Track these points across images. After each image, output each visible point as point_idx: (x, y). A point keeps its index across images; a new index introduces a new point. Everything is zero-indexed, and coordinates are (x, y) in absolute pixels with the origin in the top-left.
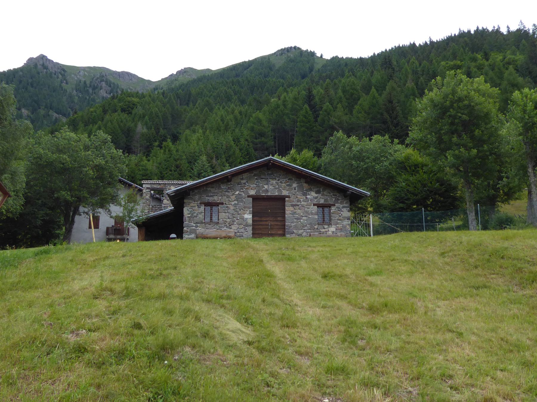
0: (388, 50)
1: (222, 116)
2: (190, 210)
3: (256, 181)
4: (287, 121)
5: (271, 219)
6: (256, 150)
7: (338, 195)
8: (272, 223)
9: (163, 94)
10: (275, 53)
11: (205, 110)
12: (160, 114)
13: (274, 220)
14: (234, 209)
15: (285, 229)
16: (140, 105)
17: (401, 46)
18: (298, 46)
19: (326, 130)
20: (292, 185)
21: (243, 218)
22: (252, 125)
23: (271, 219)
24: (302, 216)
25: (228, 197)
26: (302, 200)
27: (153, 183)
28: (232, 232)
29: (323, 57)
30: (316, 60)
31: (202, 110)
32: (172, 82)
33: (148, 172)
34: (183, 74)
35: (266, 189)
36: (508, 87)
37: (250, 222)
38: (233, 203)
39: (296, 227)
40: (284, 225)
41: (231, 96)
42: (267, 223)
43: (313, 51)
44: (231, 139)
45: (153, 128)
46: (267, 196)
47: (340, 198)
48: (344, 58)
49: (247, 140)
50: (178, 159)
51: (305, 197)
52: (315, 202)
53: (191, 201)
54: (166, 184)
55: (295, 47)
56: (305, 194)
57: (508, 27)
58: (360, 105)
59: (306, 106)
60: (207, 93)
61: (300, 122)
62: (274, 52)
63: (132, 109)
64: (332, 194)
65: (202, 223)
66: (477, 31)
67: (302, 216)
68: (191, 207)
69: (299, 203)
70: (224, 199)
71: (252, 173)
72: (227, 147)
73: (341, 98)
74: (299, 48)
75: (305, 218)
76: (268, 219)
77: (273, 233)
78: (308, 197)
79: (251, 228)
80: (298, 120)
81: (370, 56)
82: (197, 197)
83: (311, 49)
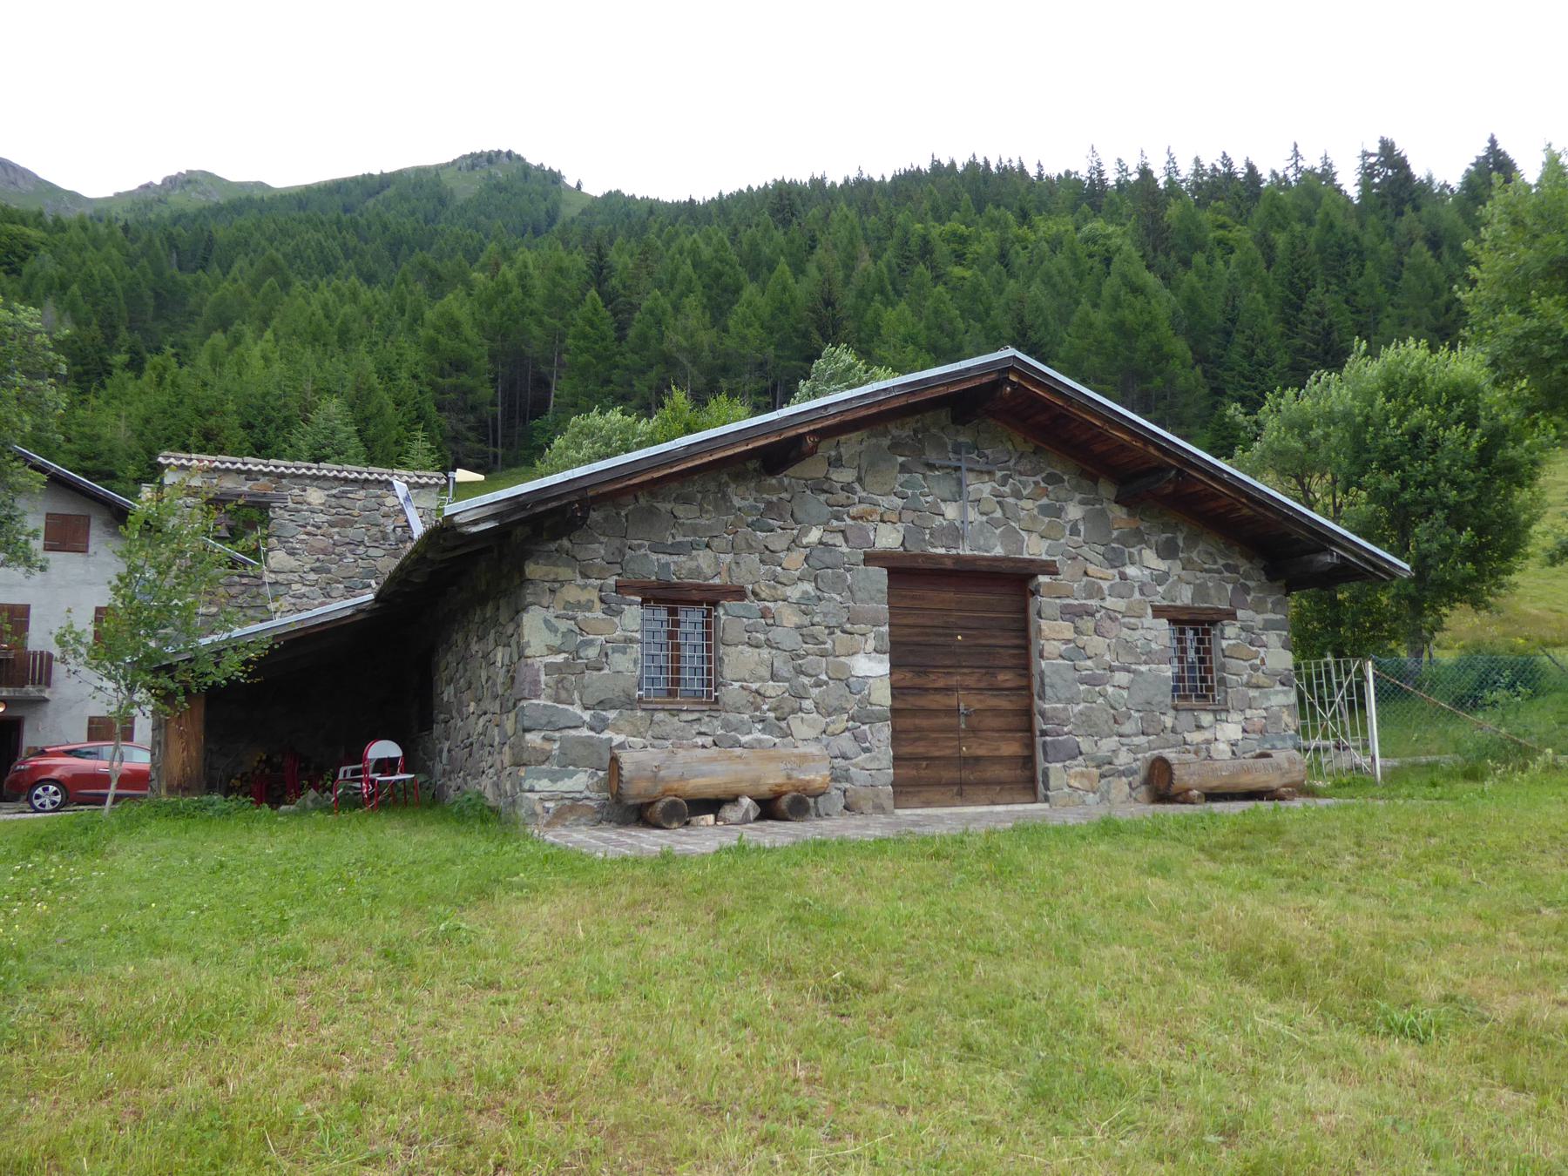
0: (755, 189)
1: (327, 304)
2: (564, 625)
3: (903, 477)
4: (536, 331)
5: (971, 681)
6: (440, 408)
7: (1244, 566)
8: (976, 702)
9: (126, 228)
10: (454, 162)
11: (266, 284)
12: (117, 285)
13: (982, 685)
14: (798, 627)
15: (1030, 729)
16: (51, 251)
17: (787, 181)
18: (517, 152)
19: (651, 366)
20: (1061, 509)
21: (845, 680)
22: (432, 332)
23: (971, 681)
24: (1111, 669)
25: (769, 555)
26: (1105, 585)
27: (216, 469)
28: (813, 758)
29: (584, 189)
30: (565, 195)
31: (255, 286)
32: (148, 205)
33: (102, 446)
34: (183, 188)
35: (952, 523)
36: (1122, 293)
37: (882, 696)
38: (794, 593)
39: (1089, 725)
40: (1028, 713)
41: (336, 259)
42: (951, 701)
43: (556, 170)
44: (371, 367)
45: (95, 321)
46: (958, 558)
47: (1251, 584)
48: (638, 197)
49: (415, 377)
50: (211, 412)
51: (1115, 571)
52: (1159, 601)
53: (564, 572)
54: (282, 476)
55: (509, 154)
56: (1115, 560)
57: (1039, 165)
58: (750, 304)
59: (593, 292)
60: (264, 243)
61: (574, 338)
62: (450, 160)
63: (23, 259)
64: (1221, 562)
65: (630, 703)
66: (972, 165)
67: (1111, 669)
68: (568, 605)
69: (1094, 603)
70: (749, 570)
71: (885, 433)
72: (358, 389)
73: (690, 281)
74: (519, 158)
75: (1122, 678)
76: (954, 681)
77: (981, 752)
78: (1131, 571)
79: (885, 731)
80: (572, 330)
81: (708, 198)
82: (598, 551)
83: (551, 163)
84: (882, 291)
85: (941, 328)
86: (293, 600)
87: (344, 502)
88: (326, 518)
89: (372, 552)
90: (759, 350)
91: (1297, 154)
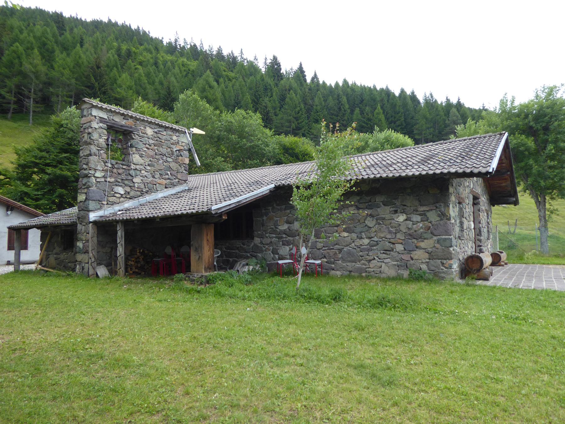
84: (117, 67)
85: (141, 86)
86: (142, 178)
87: (159, 135)
88: (153, 142)
89: (169, 159)
90: (68, 79)
91: (242, 53)
